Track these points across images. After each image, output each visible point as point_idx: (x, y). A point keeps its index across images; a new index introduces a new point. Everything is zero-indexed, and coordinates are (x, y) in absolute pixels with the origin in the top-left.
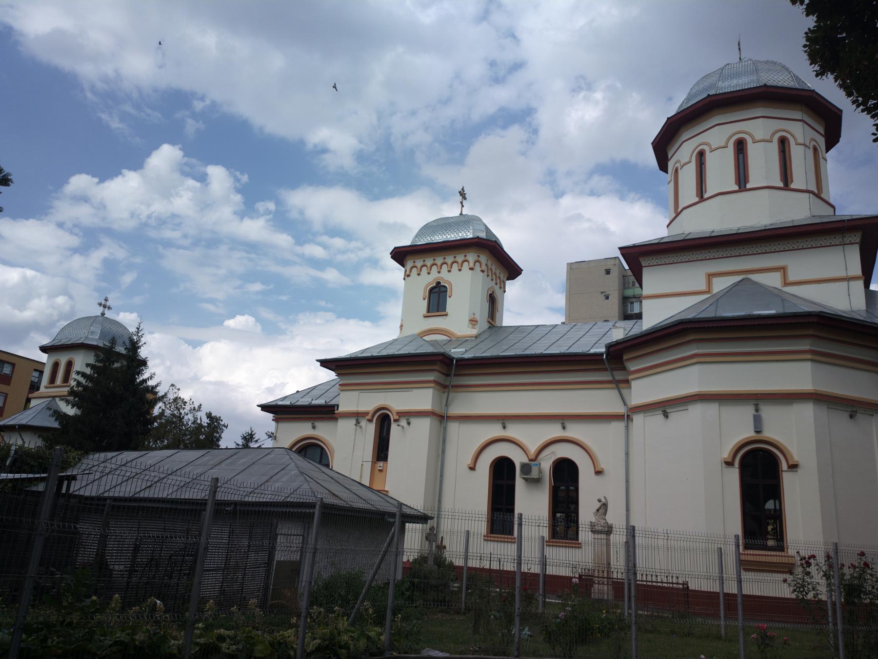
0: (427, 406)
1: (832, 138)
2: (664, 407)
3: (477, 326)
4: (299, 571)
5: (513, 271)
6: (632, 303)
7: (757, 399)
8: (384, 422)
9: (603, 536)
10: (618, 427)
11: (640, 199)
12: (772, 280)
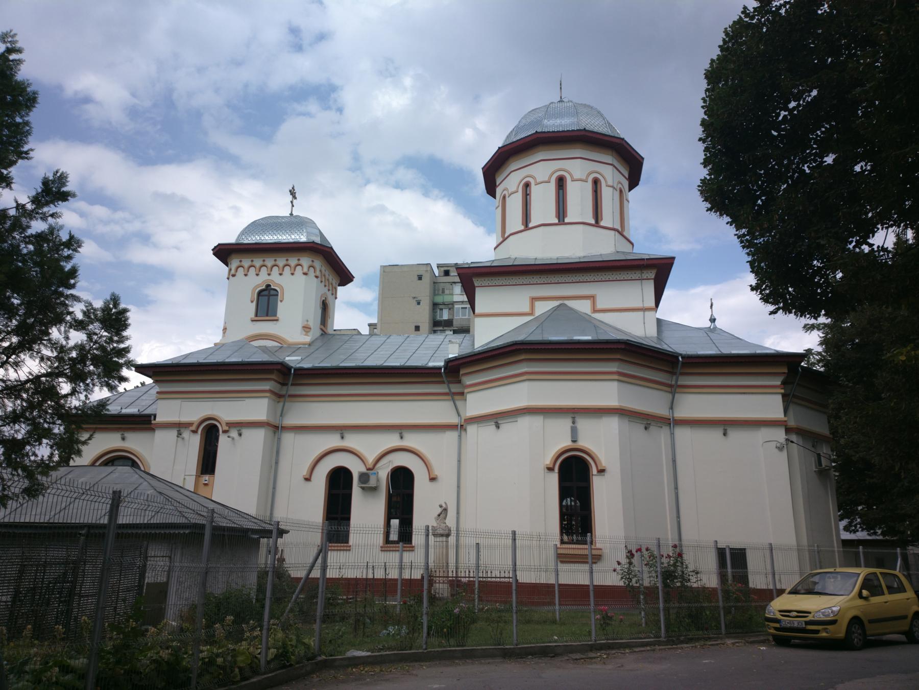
0: (262, 416)
1: (634, 181)
2: (497, 419)
3: (311, 333)
4: (166, 592)
5: (345, 277)
6: (441, 309)
7: (574, 412)
8: (211, 434)
9: (444, 539)
10: (452, 436)
11: (444, 197)
12: (583, 307)
